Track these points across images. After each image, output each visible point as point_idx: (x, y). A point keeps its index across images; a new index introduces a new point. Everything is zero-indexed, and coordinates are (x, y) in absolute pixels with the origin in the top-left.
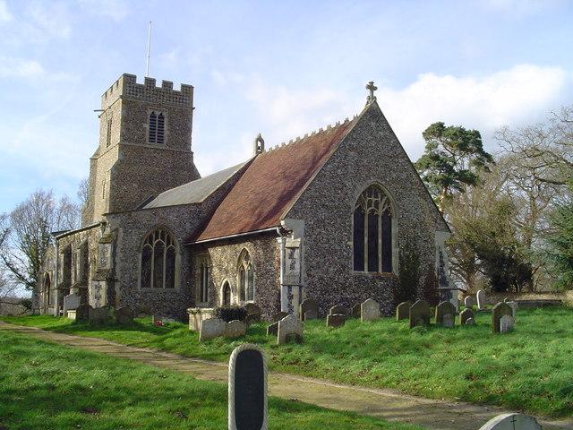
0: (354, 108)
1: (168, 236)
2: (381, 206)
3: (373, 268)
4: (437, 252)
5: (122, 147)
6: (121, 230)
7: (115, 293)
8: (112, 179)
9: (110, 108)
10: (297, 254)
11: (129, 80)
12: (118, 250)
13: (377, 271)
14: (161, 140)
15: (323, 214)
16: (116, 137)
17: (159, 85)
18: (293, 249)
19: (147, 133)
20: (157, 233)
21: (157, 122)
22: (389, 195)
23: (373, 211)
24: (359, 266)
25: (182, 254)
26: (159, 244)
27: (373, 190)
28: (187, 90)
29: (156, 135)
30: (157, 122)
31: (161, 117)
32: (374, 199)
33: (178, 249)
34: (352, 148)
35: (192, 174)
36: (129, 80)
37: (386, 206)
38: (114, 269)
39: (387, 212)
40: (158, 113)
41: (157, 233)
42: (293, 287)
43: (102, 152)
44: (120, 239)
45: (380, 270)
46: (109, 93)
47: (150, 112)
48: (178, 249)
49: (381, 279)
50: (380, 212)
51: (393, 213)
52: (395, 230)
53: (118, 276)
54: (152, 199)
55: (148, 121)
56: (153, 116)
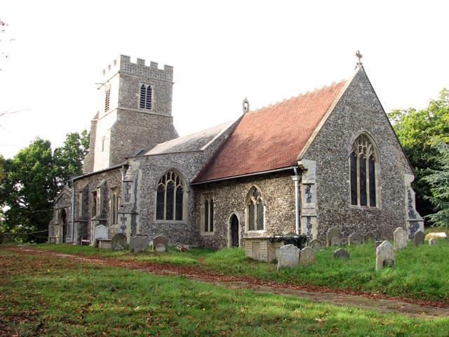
0: (349, 75)
1: (178, 178)
2: (368, 150)
3: (363, 203)
4: (406, 190)
5: (120, 111)
6: (140, 171)
7: (136, 224)
8: (112, 136)
9: (108, 81)
10: (313, 190)
11: (125, 59)
12: (138, 188)
13: (366, 205)
14: (149, 107)
15: (329, 157)
16: (114, 103)
17: (148, 64)
18: (309, 185)
19: (139, 101)
20: (169, 174)
21: (146, 93)
22: (374, 144)
23: (362, 156)
24: (354, 202)
25: (189, 192)
26: (170, 184)
27: (363, 138)
28: (169, 70)
29: (146, 101)
30: (146, 93)
31: (149, 89)
32: (363, 146)
33: (186, 188)
34: (348, 104)
35: (173, 135)
36: (125, 59)
37: (371, 152)
38: (135, 204)
39: (371, 157)
40: (147, 86)
41: (169, 174)
42: (311, 218)
43: (100, 117)
44: (140, 178)
45: (368, 204)
46: (107, 70)
47: (141, 85)
48: (186, 188)
49: (370, 212)
50: (368, 156)
51: (376, 159)
52: (377, 172)
53: (138, 211)
54: (153, 147)
55: (140, 91)
56: (143, 88)
